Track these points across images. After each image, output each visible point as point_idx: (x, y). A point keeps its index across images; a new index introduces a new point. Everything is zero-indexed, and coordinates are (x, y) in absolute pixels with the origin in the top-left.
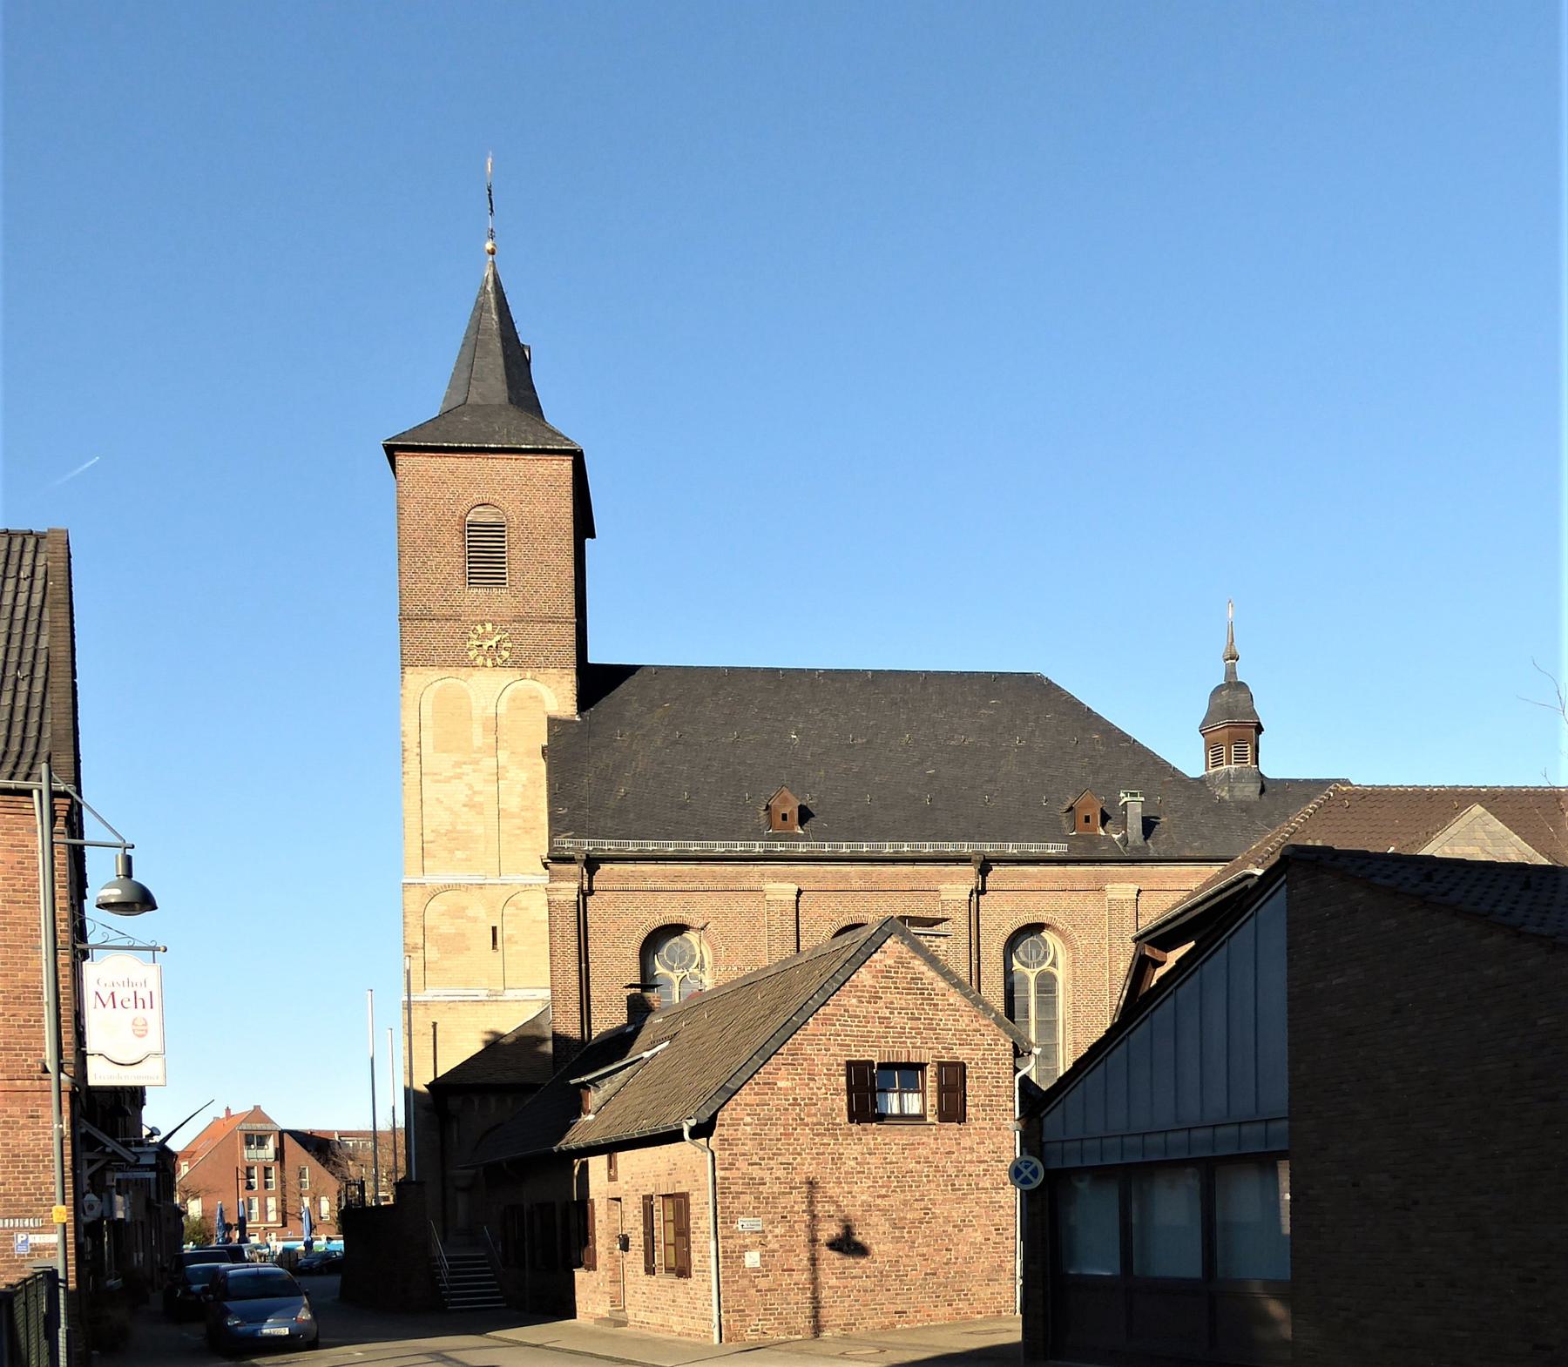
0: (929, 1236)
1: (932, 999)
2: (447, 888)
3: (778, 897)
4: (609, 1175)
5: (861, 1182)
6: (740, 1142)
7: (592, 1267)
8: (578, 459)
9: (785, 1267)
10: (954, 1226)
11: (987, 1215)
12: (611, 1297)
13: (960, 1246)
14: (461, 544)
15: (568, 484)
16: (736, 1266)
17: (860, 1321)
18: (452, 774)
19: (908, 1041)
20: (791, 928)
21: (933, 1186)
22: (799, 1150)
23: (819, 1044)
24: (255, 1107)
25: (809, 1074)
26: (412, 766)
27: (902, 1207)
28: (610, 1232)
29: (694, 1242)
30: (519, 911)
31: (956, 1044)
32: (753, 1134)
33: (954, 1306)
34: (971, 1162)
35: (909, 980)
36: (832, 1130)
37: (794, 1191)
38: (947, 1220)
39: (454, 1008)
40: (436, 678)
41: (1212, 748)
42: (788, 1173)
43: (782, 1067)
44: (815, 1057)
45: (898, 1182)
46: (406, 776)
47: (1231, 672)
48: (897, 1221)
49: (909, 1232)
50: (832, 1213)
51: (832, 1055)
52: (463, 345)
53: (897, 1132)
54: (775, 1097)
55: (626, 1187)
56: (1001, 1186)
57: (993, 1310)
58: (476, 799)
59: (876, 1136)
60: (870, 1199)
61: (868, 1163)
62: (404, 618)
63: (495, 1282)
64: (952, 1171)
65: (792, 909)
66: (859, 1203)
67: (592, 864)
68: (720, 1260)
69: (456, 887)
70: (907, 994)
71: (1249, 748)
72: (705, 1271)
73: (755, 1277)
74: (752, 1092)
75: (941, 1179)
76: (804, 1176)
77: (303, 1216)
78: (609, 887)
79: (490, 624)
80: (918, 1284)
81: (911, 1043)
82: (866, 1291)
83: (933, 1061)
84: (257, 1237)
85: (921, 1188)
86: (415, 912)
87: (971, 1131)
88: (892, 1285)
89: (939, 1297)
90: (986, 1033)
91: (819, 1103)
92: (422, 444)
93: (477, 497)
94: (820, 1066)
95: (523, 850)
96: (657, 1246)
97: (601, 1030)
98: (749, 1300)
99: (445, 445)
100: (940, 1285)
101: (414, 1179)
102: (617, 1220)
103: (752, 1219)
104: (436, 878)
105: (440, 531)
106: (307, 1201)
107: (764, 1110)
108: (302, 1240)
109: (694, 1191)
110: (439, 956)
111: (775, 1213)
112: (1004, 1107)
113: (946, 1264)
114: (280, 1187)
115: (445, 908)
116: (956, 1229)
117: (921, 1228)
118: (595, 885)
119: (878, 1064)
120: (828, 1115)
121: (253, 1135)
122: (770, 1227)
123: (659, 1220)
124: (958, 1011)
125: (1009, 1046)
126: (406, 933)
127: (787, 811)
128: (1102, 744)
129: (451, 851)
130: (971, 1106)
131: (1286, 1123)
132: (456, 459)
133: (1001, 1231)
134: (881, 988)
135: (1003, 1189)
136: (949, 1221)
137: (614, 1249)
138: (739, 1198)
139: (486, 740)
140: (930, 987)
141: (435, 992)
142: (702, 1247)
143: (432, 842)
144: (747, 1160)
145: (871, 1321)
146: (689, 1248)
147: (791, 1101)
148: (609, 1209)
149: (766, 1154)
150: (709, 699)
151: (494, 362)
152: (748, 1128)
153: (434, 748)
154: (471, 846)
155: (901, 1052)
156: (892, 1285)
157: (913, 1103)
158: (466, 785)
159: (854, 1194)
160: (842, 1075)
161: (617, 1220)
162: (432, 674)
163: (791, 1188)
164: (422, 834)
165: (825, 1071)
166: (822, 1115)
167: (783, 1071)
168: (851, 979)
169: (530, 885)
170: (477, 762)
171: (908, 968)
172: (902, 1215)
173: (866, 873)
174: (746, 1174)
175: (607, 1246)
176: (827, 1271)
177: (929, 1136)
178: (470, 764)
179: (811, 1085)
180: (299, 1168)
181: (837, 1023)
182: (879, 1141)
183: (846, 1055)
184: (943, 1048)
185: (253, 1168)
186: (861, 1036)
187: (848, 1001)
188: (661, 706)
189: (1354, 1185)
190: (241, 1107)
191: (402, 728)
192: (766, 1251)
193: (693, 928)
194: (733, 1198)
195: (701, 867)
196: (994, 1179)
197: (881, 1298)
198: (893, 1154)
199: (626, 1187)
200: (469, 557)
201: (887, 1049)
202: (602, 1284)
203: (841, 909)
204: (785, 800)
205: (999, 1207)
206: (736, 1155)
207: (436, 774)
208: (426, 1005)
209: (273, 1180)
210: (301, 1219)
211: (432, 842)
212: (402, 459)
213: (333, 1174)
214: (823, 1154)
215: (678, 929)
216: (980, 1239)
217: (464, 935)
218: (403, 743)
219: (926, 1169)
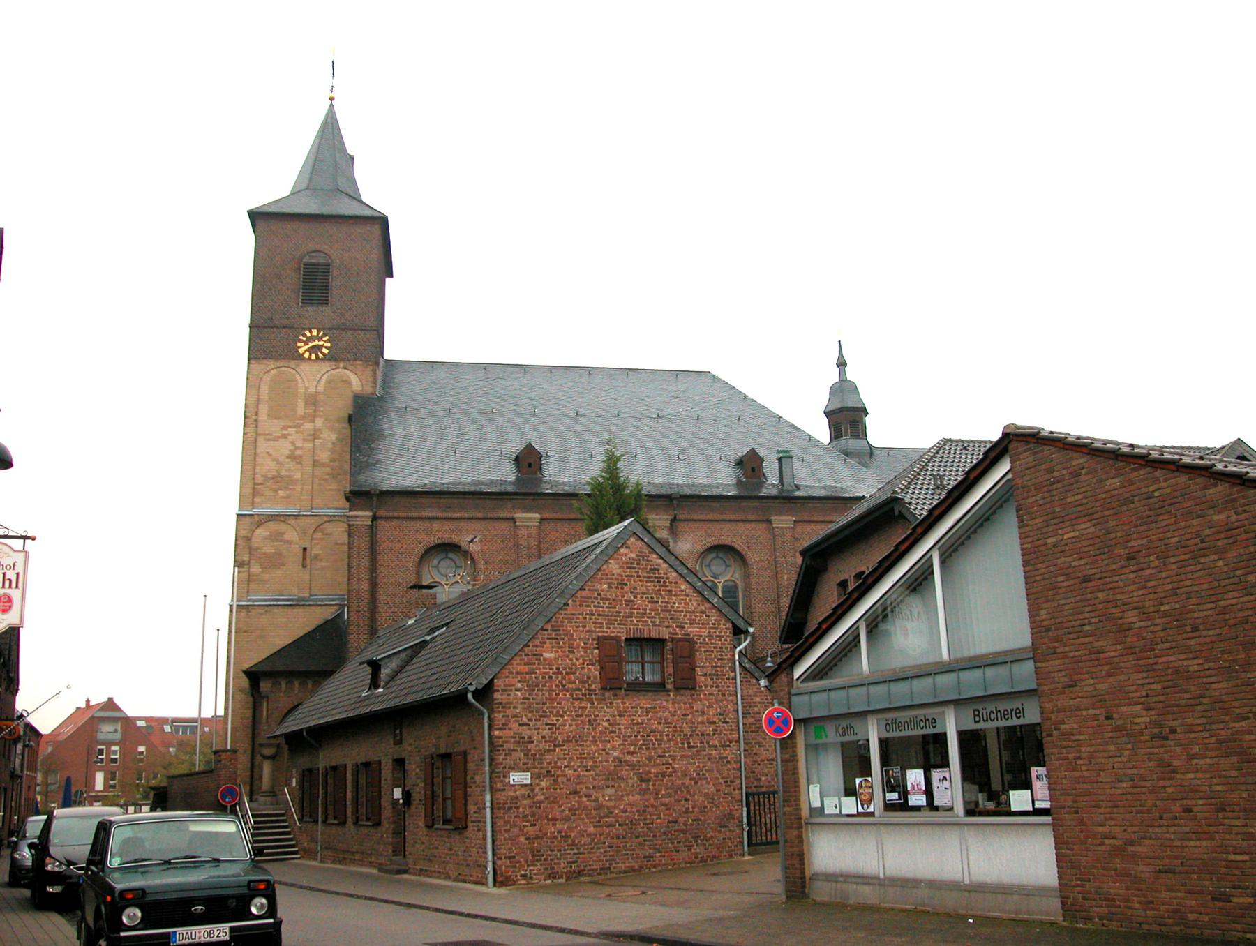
1: (667, 586)
2: (272, 518)
6: (512, 706)
10: (691, 779)
19: (649, 620)
20: (535, 547)
29: (470, 795)
31: (687, 623)
32: (523, 699)
33: (693, 851)
34: (703, 723)
38: (685, 775)
40: (273, 367)
42: (552, 733)
45: (644, 741)
55: (409, 749)
56: (728, 743)
60: (621, 756)
61: (619, 724)
64: (687, 731)
70: (647, 582)
72: (479, 821)
73: (524, 826)
74: (523, 662)
82: (618, 838)
87: (702, 696)
90: (710, 614)
98: (519, 848)
100: (681, 831)
101: (229, 747)
111: (542, 768)
120: (585, 682)
122: (537, 781)
124: (688, 596)
131: (1030, 665)
135: (729, 746)
143: (261, 484)
147: (555, 670)
152: (519, 693)
153: (269, 415)
154: (291, 487)
158: (291, 442)
160: (595, 648)
163: (555, 746)
171: (648, 560)
174: (517, 734)
176: (586, 820)
177: (667, 701)
179: (571, 657)
184: (677, 627)
189: (1108, 718)
190: (98, 698)
192: (534, 803)
196: (722, 738)
199: (409, 749)
201: (632, 627)
203: (573, 532)
205: (727, 762)
211: (261, 484)
214: (582, 716)
219: (666, 730)
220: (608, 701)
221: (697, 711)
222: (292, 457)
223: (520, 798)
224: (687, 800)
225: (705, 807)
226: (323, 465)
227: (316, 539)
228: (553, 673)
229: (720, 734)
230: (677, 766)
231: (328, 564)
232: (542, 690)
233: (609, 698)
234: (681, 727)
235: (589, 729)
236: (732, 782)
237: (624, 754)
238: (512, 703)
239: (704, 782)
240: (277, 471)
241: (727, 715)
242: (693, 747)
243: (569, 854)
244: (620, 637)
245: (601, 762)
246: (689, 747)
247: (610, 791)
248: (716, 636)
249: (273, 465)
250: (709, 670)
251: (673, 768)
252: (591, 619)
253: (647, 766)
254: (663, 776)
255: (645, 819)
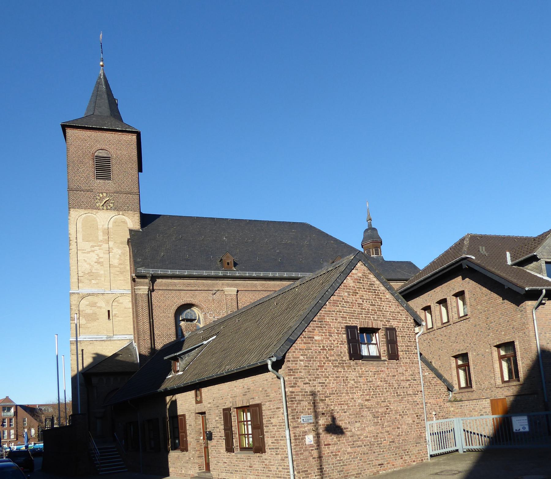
0: (390, 421)
2: (89, 295)
3: (229, 293)
4: (196, 400)
5: (357, 393)
6: (298, 371)
7: (185, 449)
8: (138, 134)
9: (326, 443)
11: (413, 409)
12: (199, 465)
13: (403, 426)
14: (93, 163)
15: (135, 144)
16: (302, 444)
17: (363, 471)
18: (90, 250)
19: (371, 316)
21: (389, 393)
22: (327, 375)
23: (332, 317)
24: (6, 397)
25: (329, 333)
26: (73, 247)
27: (376, 405)
28: (197, 430)
30: (119, 304)
31: (391, 319)
34: (403, 380)
35: (369, 285)
36: (342, 364)
37: (327, 399)
38: (396, 412)
39: (92, 343)
41: (366, 250)
42: (323, 389)
43: (316, 328)
44: (331, 323)
45: (374, 392)
46: (71, 251)
47: (370, 225)
48: (375, 414)
49: (381, 419)
50: (345, 411)
51: (339, 323)
52: (92, 96)
53: (371, 365)
54: (314, 345)
55: (209, 405)
56: (417, 393)
57: (419, 459)
58: (100, 260)
59: (362, 367)
60: (362, 402)
62: (70, 190)
63: (121, 459)
65: (235, 297)
66: (357, 404)
67: (154, 279)
68: (292, 441)
69: (93, 294)
70: (369, 292)
71: (379, 250)
75: (392, 390)
76: (331, 390)
77: (25, 436)
78: (161, 288)
79: (105, 194)
80: (387, 448)
81: (373, 317)
83: (383, 328)
84: (6, 445)
85: (384, 395)
86: (75, 304)
87: (402, 364)
88: (376, 450)
89: (397, 454)
91: (335, 349)
92: (74, 125)
93: (99, 146)
94: (334, 329)
95: (120, 280)
96: (235, 436)
97: (168, 342)
99: (86, 126)
100: (397, 447)
102: (200, 424)
103: (307, 416)
104: (84, 290)
105: (84, 158)
106: (26, 430)
107: (309, 352)
108: (24, 445)
109: (266, 402)
110: (86, 322)
112: (413, 352)
113: (398, 436)
114: (15, 426)
115: (88, 303)
116: (401, 417)
117: (385, 417)
118: (155, 288)
119: (360, 328)
121: (6, 407)
123: (235, 421)
125: (412, 321)
126: (71, 313)
127: (229, 261)
128: (335, 244)
129: (90, 280)
130: (400, 351)
132: (90, 132)
133: (419, 417)
134: (358, 288)
136: (397, 412)
137: (199, 439)
138: (300, 403)
139: (104, 237)
140: (378, 289)
141: (85, 337)
142: (275, 434)
143: (82, 277)
144: (303, 381)
145: (368, 471)
146: (264, 435)
147: (322, 348)
148: (196, 419)
149: (312, 377)
150: (190, 226)
151: (104, 101)
152: (302, 363)
153: (83, 240)
155: (369, 322)
156: (376, 450)
157: (373, 351)
159: (355, 399)
160: (344, 334)
161: (200, 424)
162: (82, 211)
164: (78, 273)
165: (336, 331)
166: (337, 355)
167: (316, 331)
168: (344, 282)
169: (123, 294)
170: (101, 246)
171: (368, 278)
172: (377, 410)
173: (263, 284)
175: (195, 438)
176: (346, 444)
177: (384, 367)
178: (98, 246)
180: (23, 418)
181: (340, 306)
182: (363, 370)
183: (345, 323)
184: (387, 321)
185: (5, 419)
186: (351, 313)
187: (344, 294)
188: (173, 228)
191: (69, 232)
193: (196, 305)
194: (297, 404)
195: (198, 281)
196: (413, 389)
197: (372, 457)
198: (370, 377)
199: (209, 405)
200: (96, 168)
201: (363, 320)
202: (192, 458)
204: (228, 257)
206: (297, 378)
207: (83, 250)
208: (80, 342)
209: (13, 423)
210: (24, 437)
211: (82, 277)
212: (69, 131)
213: (36, 420)
214: (339, 377)
215: (189, 306)
216: (411, 422)
217: (96, 314)
218: (70, 237)
219: (385, 385)
220: (353, 368)
221: (400, 373)
222: (98, 262)
223: (308, 432)
224: (398, 428)
225: (408, 432)
226: (115, 267)
227: (115, 306)
228: (321, 350)
229: (412, 387)
230: (392, 407)
231: (122, 319)
232: (315, 361)
233: (354, 366)
234: (392, 383)
235: (343, 386)
236: (420, 416)
237: (363, 401)
238: (298, 369)
239: (406, 416)
240: (90, 269)
241: (415, 375)
242: (400, 395)
243: (338, 466)
244: (357, 326)
245: (352, 406)
246: (397, 396)
247: (358, 425)
248: (407, 327)
249: (88, 267)
250: (404, 348)
251: (390, 409)
252: (340, 315)
253: (376, 407)
254: (385, 414)
255: (378, 441)
